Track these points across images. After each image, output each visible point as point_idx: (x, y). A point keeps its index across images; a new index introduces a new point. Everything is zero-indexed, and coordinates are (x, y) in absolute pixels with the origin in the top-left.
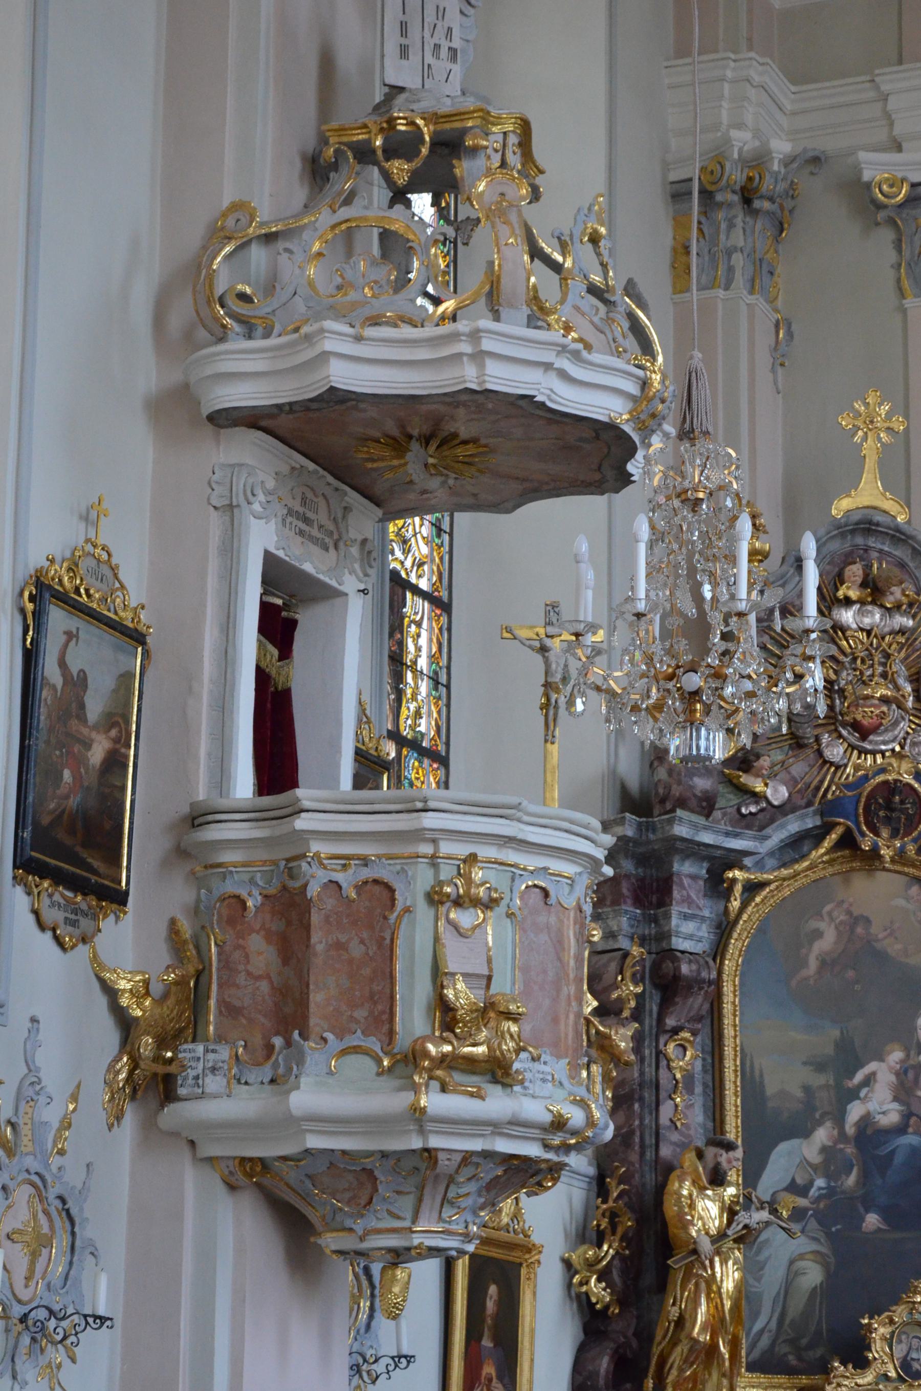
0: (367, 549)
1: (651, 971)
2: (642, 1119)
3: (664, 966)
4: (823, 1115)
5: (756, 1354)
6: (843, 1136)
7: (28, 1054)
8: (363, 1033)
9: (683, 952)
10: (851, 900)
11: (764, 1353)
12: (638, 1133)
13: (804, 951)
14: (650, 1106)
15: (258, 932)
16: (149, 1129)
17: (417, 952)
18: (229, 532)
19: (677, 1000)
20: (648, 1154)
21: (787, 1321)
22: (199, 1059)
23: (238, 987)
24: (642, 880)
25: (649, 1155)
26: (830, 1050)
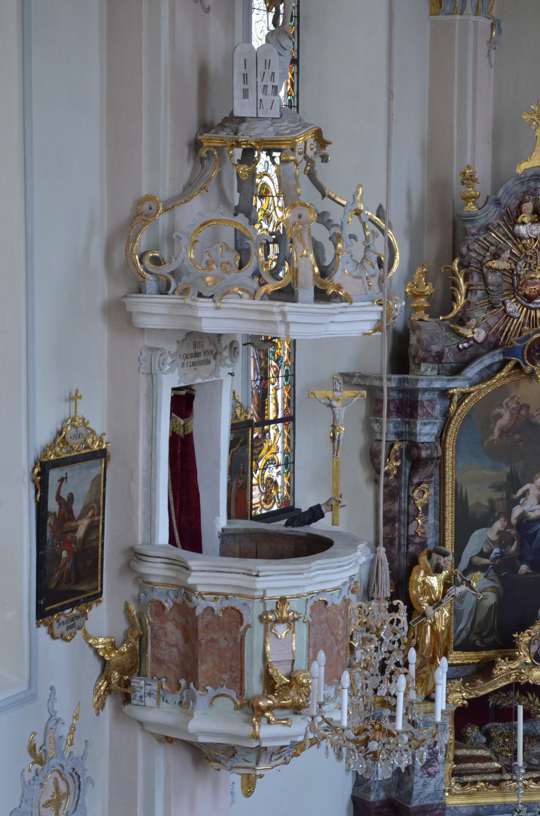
0: (234, 346)
1: (405, 450)
2: (399, 531)
3: (413, 451)
4: (499, 515)
5: (459, 641)
6: (509, 525)
7: (50, 708)
8: (227, 686)
9: (423, 443)
10: (519, 396)
11: (463, 641)
12: (397, 539)
13: (492, 426)
14: (404, 524)
15: (171, 621)
16: (119, 715)
17: (254, 648)
18: (151, 385)
19: (419, 470)
20: (403, 549)
21: (477, 623)
22: (142, 688)
23: (161, 649)
24: (401, 400)
25: (403, 549)
26: (505, 479)
